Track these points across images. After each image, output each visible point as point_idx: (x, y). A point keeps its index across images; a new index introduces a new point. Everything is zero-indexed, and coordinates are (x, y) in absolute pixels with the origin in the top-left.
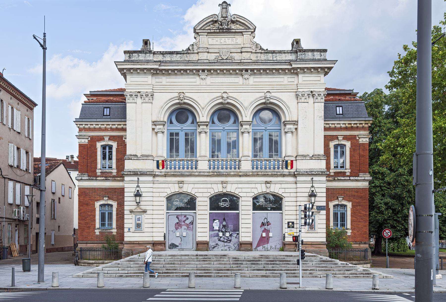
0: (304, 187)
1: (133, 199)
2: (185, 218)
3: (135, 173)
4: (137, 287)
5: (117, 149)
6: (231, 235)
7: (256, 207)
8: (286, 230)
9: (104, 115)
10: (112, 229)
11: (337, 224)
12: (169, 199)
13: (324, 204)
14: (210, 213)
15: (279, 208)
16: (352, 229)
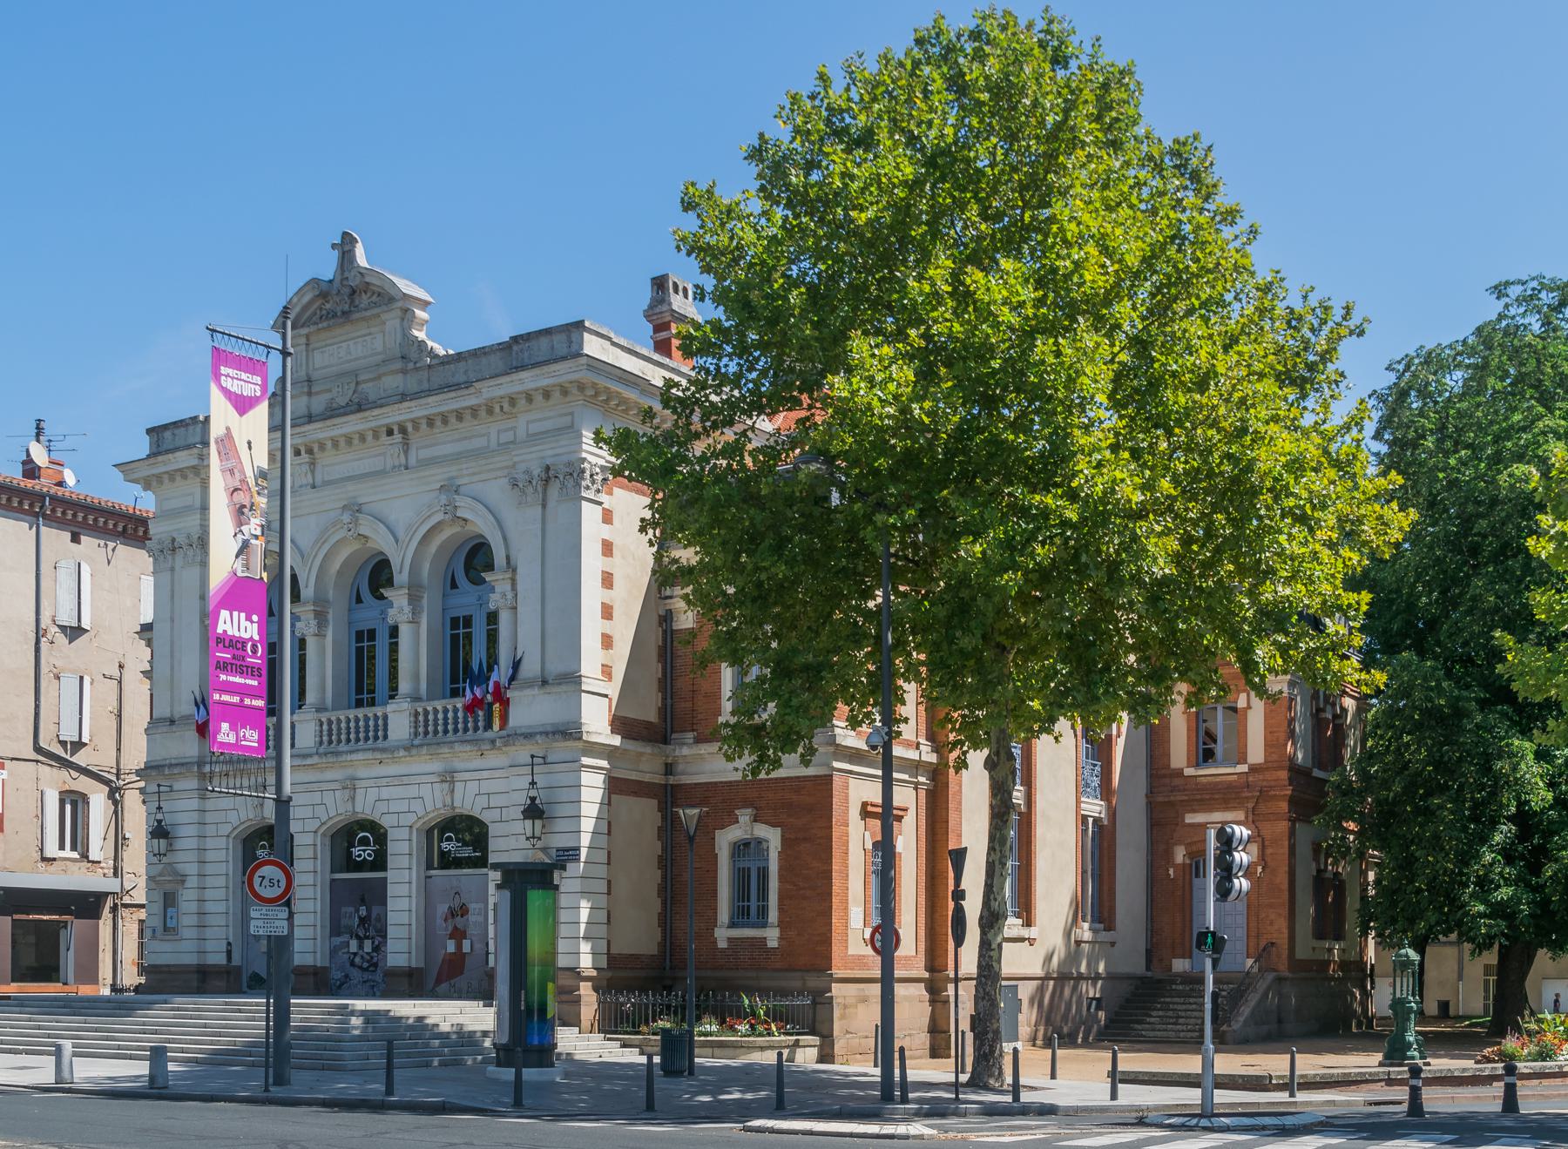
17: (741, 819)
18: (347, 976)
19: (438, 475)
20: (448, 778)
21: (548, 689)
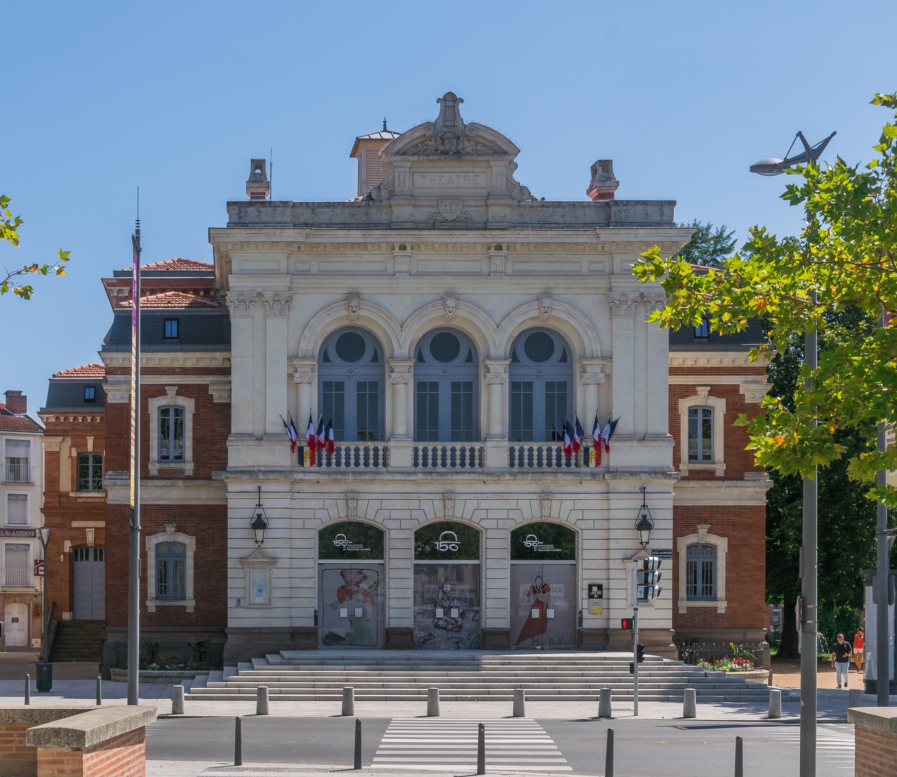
0: (625, 508)
1: (249, 533)
2: (360, 577)
3: (250, 473)
4: (327, 715)
5: (196, 418)
6: (462, 615)
7: (519, 551)
8: (584, 603)
9: (165, 338)
10: (184, 598)
11: (695, 587)
12: (327, 535)
13: (669, 545)
14: (416, 565)
15: (571, 554)
16: (727, 598)
17: (168, 529)
18: (430, 635)
19: (537, 286)
20: (447, 496)
21: (645, 443)
